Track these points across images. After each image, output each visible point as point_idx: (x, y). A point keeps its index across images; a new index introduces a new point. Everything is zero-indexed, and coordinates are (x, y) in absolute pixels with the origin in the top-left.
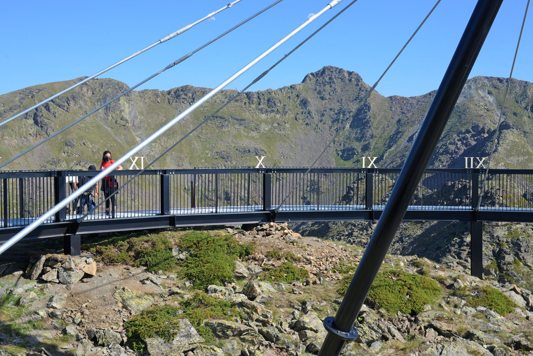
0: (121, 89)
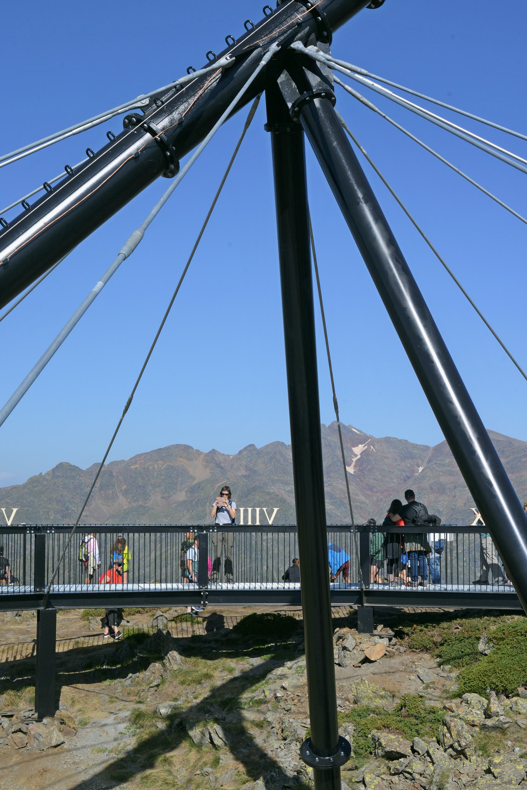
0: (186, 450)
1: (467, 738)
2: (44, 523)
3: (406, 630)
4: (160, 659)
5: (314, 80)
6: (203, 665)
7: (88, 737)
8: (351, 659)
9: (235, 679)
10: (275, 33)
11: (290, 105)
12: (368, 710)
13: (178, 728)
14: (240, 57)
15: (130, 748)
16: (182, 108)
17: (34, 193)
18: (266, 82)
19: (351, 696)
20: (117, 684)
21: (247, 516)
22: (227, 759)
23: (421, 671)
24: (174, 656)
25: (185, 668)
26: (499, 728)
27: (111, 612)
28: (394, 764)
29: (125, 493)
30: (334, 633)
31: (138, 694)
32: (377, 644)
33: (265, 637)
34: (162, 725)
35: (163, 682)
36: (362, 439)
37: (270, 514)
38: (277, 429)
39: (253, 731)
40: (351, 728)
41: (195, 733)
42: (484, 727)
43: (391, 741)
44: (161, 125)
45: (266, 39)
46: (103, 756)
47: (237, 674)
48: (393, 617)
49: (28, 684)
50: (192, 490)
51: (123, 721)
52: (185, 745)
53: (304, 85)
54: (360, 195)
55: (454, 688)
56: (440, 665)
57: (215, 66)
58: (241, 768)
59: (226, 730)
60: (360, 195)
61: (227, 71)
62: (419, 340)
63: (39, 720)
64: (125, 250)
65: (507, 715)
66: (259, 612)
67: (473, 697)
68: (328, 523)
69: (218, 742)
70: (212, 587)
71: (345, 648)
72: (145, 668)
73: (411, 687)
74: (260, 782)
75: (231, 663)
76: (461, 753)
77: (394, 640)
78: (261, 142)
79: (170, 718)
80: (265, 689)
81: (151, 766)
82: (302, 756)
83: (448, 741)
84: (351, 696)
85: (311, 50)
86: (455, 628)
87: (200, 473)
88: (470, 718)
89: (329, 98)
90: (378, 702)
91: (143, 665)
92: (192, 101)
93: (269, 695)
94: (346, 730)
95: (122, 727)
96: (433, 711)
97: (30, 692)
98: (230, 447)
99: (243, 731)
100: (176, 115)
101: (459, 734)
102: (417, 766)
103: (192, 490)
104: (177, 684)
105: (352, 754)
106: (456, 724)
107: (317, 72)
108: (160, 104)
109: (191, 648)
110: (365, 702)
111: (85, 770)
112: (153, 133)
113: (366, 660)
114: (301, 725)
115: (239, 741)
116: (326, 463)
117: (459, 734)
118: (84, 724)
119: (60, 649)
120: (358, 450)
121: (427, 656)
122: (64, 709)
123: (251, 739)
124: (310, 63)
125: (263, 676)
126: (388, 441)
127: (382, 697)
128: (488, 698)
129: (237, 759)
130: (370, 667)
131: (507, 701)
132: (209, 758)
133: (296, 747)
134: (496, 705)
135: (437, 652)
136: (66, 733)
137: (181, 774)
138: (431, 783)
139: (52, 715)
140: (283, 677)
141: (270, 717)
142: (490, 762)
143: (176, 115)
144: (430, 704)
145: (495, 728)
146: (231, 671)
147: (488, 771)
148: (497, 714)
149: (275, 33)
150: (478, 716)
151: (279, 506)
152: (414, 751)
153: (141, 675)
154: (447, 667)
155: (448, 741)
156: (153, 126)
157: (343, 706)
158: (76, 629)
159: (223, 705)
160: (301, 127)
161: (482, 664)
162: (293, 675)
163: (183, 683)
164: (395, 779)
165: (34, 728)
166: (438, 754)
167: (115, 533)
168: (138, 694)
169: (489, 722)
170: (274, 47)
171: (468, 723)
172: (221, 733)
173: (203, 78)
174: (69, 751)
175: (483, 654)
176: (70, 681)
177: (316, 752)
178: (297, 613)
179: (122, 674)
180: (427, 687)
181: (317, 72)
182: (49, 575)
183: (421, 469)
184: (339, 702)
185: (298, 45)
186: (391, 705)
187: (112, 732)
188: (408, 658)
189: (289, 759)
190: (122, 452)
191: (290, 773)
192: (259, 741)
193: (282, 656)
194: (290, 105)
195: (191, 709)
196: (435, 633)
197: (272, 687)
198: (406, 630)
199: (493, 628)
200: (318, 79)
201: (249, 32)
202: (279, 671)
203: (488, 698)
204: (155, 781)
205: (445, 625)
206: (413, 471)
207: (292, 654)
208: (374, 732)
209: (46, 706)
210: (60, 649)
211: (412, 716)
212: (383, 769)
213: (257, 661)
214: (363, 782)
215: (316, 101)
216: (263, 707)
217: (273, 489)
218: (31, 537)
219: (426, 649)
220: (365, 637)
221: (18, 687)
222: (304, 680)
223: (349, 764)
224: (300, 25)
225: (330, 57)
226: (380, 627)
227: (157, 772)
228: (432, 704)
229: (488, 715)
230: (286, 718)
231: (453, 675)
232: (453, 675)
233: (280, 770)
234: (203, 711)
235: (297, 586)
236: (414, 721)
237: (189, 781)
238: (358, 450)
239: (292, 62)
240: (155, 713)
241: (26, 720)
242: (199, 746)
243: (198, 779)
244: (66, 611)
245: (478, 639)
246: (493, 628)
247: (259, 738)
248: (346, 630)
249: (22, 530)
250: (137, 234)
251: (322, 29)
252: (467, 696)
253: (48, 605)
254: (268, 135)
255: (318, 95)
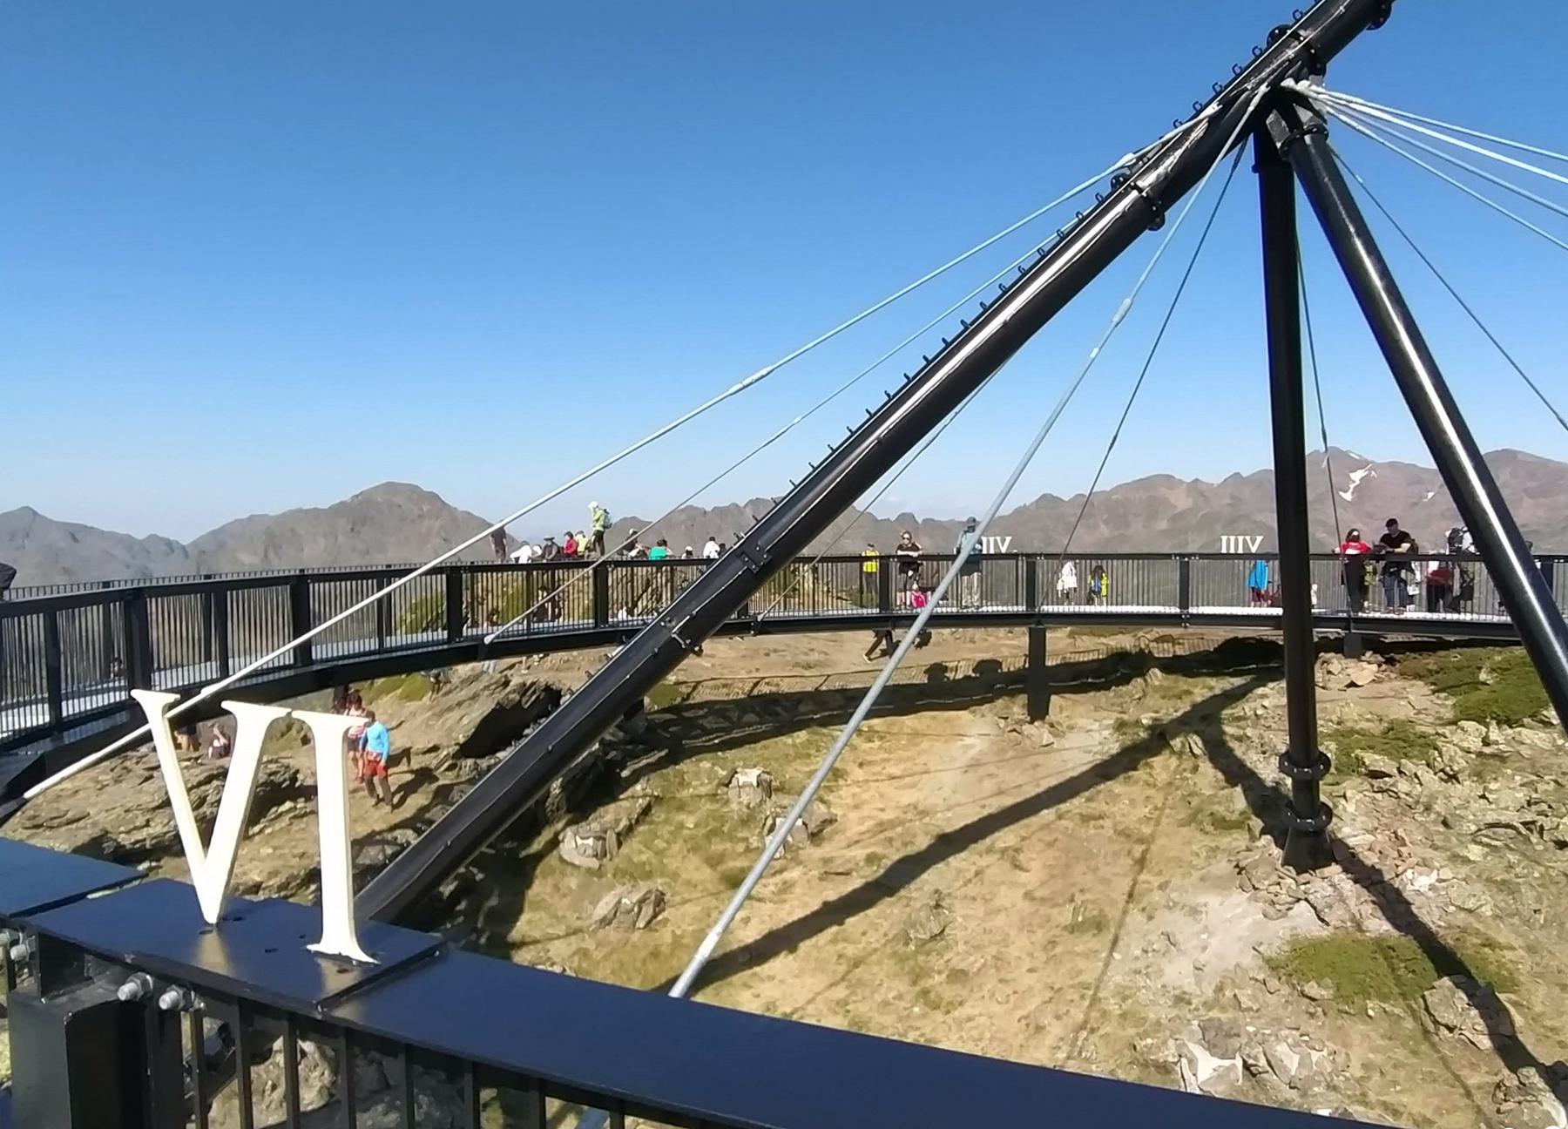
1: (1460, 763)
2: (1190, 550)
3: (1398, 657)
4: (1142, 675)
5: (1305, 116)
6: (1183, 683)
7: (1073, 740)
8: (1336, 683)
9: (1215, 696)
10: (1263, 75)
11: (1279, 145)
12: (1352, 731)
13: (1160, 738)
14: (1227, 104)
15: (1114, 752)
16: (1168, 162)
17: (1028, 258)
18: (1256, 125)
19: (1334, 718)
20: (1101, 696)
21: (1230, 543)
22: (1206, 767)
23: (1412, 698)
24: (1156, 676)
25: (1165, 684)
26: (1500, 757)
27: (912, 843)
28: (1376, 783)
29: (1106, 523)
30: (1317, 658)
31: (1121, 705)
32: (1365, 670)
33: (1244, 658)
34: (1143, 735)
35: (1145, 695)
36: (1362, 464)
37: (1253, 542)
38: (1261, 457)
39: (1233, 744)
40: (1333, 746)
41: (1177, 743)
42: (1480, 754)
43: (1374, 760)
44: (1147, 182)
45: (1254, 81)
46: (1090, 757)
47: (1218, 691)
48: (1387, 646)
49: (1021, 691)
50: (1174, 519)
51: (1107, 727)
52: (1167, 752)
53: (1294, 122)
54: (1352, 230)
55: (1449, 715)
56: (1434, 692)
57: (1201, 116)
58: (1220, 776)
59: (1205, 743)
60: (1352, 230)
61: (1213, 119)
62: (1412, 372)
63: (1032, 722)
64: (1116, 319)
65: (1508, 743)
66: (1240, 636)
67: (1470, 725)
68: (1312, 551)
69: (1197, 751)
70: (1193, 610)
71: (1329, 672)
72: (1128, 683)
73: (1400, 711)
74: (1239, 789)
75: (1212, 681)
76: (1453, 778)
77: (1384, 667)
78: (1248, 186)
79: (1150, 728)
80: (1246, 707)
81: (1135, 769)
82: (1282, 769)
83: (1439, 764)
84: (1334, 718)
85: (1302, 86)
86: (1455, 656)
87: (1182, 502)
88: (1465, 745)
89: (1320, 132)
90: (1364, 725)
91: (1125, 680)
92: (1179, 152)
93: (1250, 713)
94: (1329, 748)
95: (1106, 733)
96: (1424, 736)
97: (1023, 699)
98: (1214, 474)
99: (1223, 743)
100: (1161, 170)
101: (1451, 759)
102: (1403, 786)
103: (1174, 519)
104: (1155, 699)
105: (1333, 770)
106: (1449, 750)
107: (1309, 107)
108: (1146, 162)
109: (1173, 666)
110: (1349, 724)
111: (1073, 769)
112: (1140, 190)
113: (1352, 685)
114: (1281, 742)
115: (1219, 753)
116: (1311, 495)
117: (1451, 759)
118: (1071, 728)
119: (1049, 663)
120: (1357, 476)
121: (1420, 683)
122: (1053, 716)
123: (1231, 750)
124: (1304, 101)
125: (1244, 695)
126: (1392, 464)
127: (1368, 720)
128: (1487, 725)
129: (1216, 767)
130: (1352, 690)
131: (1510, 731)
132: (1188, 764)
133: (1275, 761)
134: (1495, 734)
135: (1432, 679)
136: (1055, 736)
137: (1162, 777)
138: (1417, 802)
139: (1043, 718)
140: (1263, 696)
141: (1249, 732)
142: (1485, 789)
143: (1161, 170)
144: (1419, 729)
145: (1493, 756)
146: (1211, 688)
147: (1483, 797)
148: (1497, 743)
149: (1263, 75)
150: (1475, 743)
151: (1260, 537)
152: (1400, 772)
153: (1123, 689)
154: (1443, 695)
155: (1439, 764)
156: (1140, 183)
157: (1323, 726)
158: (1061, 645)
159: (1204, 720)
160: (1292, 165)
161: (1483, 693)
162: (1272, 697)
163: (1163, 697)
164: (1379, 796)
165: (1027, 729)
166: (1427, 776)
167: (1094, 562)
168: (1121, 705)
169: (1487, 750)
170: (1263, 89)
171: (1462, 749)
172: (1200, 743)
173: (1191, 129)
174: (1058, 750)
175: (1484, 683)
176: (1059, 691)
177: (1294, 763)
178: (1277, 636)
179: (1106, 687)
180: (1419, 712)
181: (1309, 107)
182: (1040, 598)
183: (1430, 495)
184: (1320, 722)
185: (1288, 83)
186: (1377, 728)
187: (1097, 737)
188: (1398, 684)
189: (1269, 771)
190: (1105, 485)
191: (1269, 784)
192: (1239, 752)
193: (1263, 678)
194: (1279, 145)
195: (1172, 721)
196: (1430, 661)
197: (1253, 705)
198: (1398, 657)
199: (1498, 658)
200: (1310, 114)
201: (1238, 76)
202: (1260, 691)
203: (1487, 725)
204: (1136, 782)
205: (1442, 653)
206: (1421, 498)
207: (1273, 676)
208: (1358, 752)
209: (1038, 711)
210: (1049, 663)
211: (1402, 740)
212: (1366, 786)
213: (1238, 681)
214: (1344, 797)
215: (1307, 138)
216: (1242, 723)
217: (1259, 517)
218: (1022, 565)
219: (1418, 676)
220: (1351, 663)
221: (1012, 694)
222: (1284, 700)
223: (1328, 778)
224: (1291, 62)
225: (1320, 90)
226: (1368, 654)
227: (1140, 774)
228: (1424, 729)
229: (1486, 742)
230: (1265, 734)
231: (1450, 702)
232: (1450, 702)
233: (1260, 781)
234: (1184, 724)
235: (1279, 611)
236: (1402, 744)
237: (1170, 784)
238: (1357, 476)
239: (1283, 101)
240: (1138, 723)
241: (1020, 722)
242: (1180, 754)
243: (1177, 783)
244: (1055, 629)
245: (1480, 668)
246: (1498, 658)
247: (1238, 750)
248: (1332, 654)
249: (1014, 556)
250: (1128, 301)
251: (1314, 63)
252: (1462, 723)
253: (1039, 623)
254: (1255, 178)
255: (1309, 132)
